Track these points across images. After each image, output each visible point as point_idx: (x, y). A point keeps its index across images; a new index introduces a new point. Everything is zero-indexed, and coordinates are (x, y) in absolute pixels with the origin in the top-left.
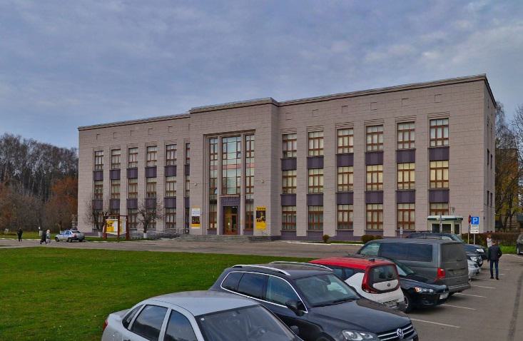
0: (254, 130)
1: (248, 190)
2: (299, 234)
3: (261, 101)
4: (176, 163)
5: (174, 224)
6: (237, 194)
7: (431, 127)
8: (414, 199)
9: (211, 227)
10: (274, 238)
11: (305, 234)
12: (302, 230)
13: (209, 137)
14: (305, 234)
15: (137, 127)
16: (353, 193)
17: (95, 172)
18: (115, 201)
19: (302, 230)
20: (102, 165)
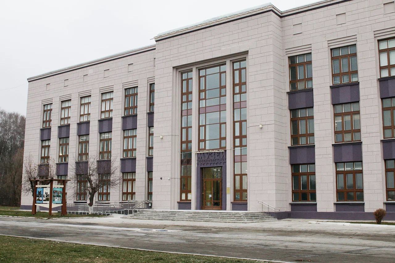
0: (246, 53)
1: (237, 141)
2: (320, 208)
3: (187, 29)
4: (112, 115)
5: (133, 194)
6: (221, 148)
7: (381, 51)
8: (361, 157)
9: (184, 197)
10: (280, 216)
11: (331, 209)
12: (326, 198)
13: (182, 70)
14: (331, 209)
15: (90, 70)
16: (360, 143)
17: (42, 130)
18: (63, 165)
19: (326, 198)
20: (89, 114)
